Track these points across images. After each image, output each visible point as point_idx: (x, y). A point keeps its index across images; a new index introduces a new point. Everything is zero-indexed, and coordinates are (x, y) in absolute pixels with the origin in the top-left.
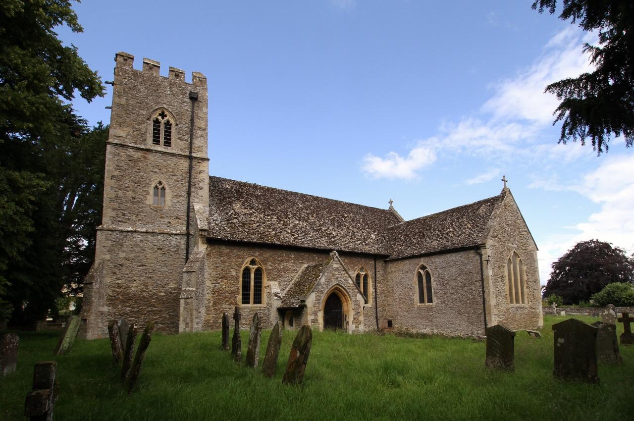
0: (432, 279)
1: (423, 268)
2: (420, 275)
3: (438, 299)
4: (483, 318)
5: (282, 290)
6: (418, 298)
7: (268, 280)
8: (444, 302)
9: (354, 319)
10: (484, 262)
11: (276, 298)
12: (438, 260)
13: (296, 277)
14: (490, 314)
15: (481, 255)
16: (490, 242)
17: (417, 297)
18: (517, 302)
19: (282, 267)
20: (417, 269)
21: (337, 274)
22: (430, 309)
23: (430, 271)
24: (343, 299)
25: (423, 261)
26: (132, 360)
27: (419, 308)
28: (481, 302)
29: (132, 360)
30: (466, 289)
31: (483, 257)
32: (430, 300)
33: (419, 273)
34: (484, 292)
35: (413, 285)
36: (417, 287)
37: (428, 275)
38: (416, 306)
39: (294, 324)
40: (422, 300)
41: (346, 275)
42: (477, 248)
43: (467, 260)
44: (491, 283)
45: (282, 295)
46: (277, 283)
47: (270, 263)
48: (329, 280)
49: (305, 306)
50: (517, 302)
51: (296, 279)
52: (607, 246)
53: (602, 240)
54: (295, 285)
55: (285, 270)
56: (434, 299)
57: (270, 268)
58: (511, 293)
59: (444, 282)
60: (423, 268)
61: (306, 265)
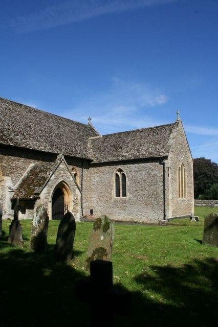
0: (127, 179)
1: (120, 170)
2: (117, 175)
3: (131, 194)
4: (163, 208)
5: (14, 183)
6: (115, 193)
7: (3, 175)
8: (135, 196)
9: (74, 208)
10: (166, 169)
11: (10, 190)
12: (133, 167)
13: (25, 174)
14: (168, 205)
15: (164, 164)
16: (170, 155)
17: (114, 192)
18: (182, 197)
19: (14, 165)
20: (115, 171)
21: (62, 172)
22: (125, 202)
23: (125, 174)
24: (65, 192)
25: (120, 167)
26: (3, 242)
27: (116, 201)
28: (162, 196)
29: (3, 242)
30: (152, 187)
31: (166, 165)
32: (124, 195)
33: (117, 175)
34: (164, 190)
35: (111, 183)
36: (114, 185)
37: (124, 175)
38: (113, 199)
39: (26, 212)
40: (118, 195)
41: (69, 174)
42: (161, 160)
43: (155, 167)
44: (170, 183)
45: (15, 187)
46: (10, 178)
47: (5, 161)
48: (57, 178)
49: (39, 198)
50: (182, 197)
51: (25, 175)
52: (210, 160)
53: (207, 158)
54: (24, 180)
55: (17, 168)
56: (128, 194)
57: (5, 165)
58: (179, 190)
59: (136, 182)
60: (120, 170)
61: (32, 165)
